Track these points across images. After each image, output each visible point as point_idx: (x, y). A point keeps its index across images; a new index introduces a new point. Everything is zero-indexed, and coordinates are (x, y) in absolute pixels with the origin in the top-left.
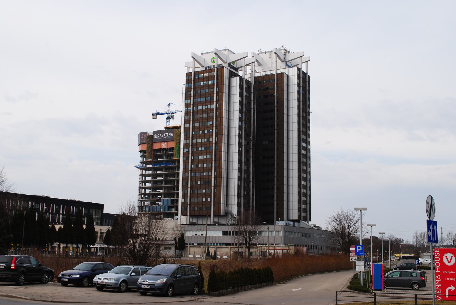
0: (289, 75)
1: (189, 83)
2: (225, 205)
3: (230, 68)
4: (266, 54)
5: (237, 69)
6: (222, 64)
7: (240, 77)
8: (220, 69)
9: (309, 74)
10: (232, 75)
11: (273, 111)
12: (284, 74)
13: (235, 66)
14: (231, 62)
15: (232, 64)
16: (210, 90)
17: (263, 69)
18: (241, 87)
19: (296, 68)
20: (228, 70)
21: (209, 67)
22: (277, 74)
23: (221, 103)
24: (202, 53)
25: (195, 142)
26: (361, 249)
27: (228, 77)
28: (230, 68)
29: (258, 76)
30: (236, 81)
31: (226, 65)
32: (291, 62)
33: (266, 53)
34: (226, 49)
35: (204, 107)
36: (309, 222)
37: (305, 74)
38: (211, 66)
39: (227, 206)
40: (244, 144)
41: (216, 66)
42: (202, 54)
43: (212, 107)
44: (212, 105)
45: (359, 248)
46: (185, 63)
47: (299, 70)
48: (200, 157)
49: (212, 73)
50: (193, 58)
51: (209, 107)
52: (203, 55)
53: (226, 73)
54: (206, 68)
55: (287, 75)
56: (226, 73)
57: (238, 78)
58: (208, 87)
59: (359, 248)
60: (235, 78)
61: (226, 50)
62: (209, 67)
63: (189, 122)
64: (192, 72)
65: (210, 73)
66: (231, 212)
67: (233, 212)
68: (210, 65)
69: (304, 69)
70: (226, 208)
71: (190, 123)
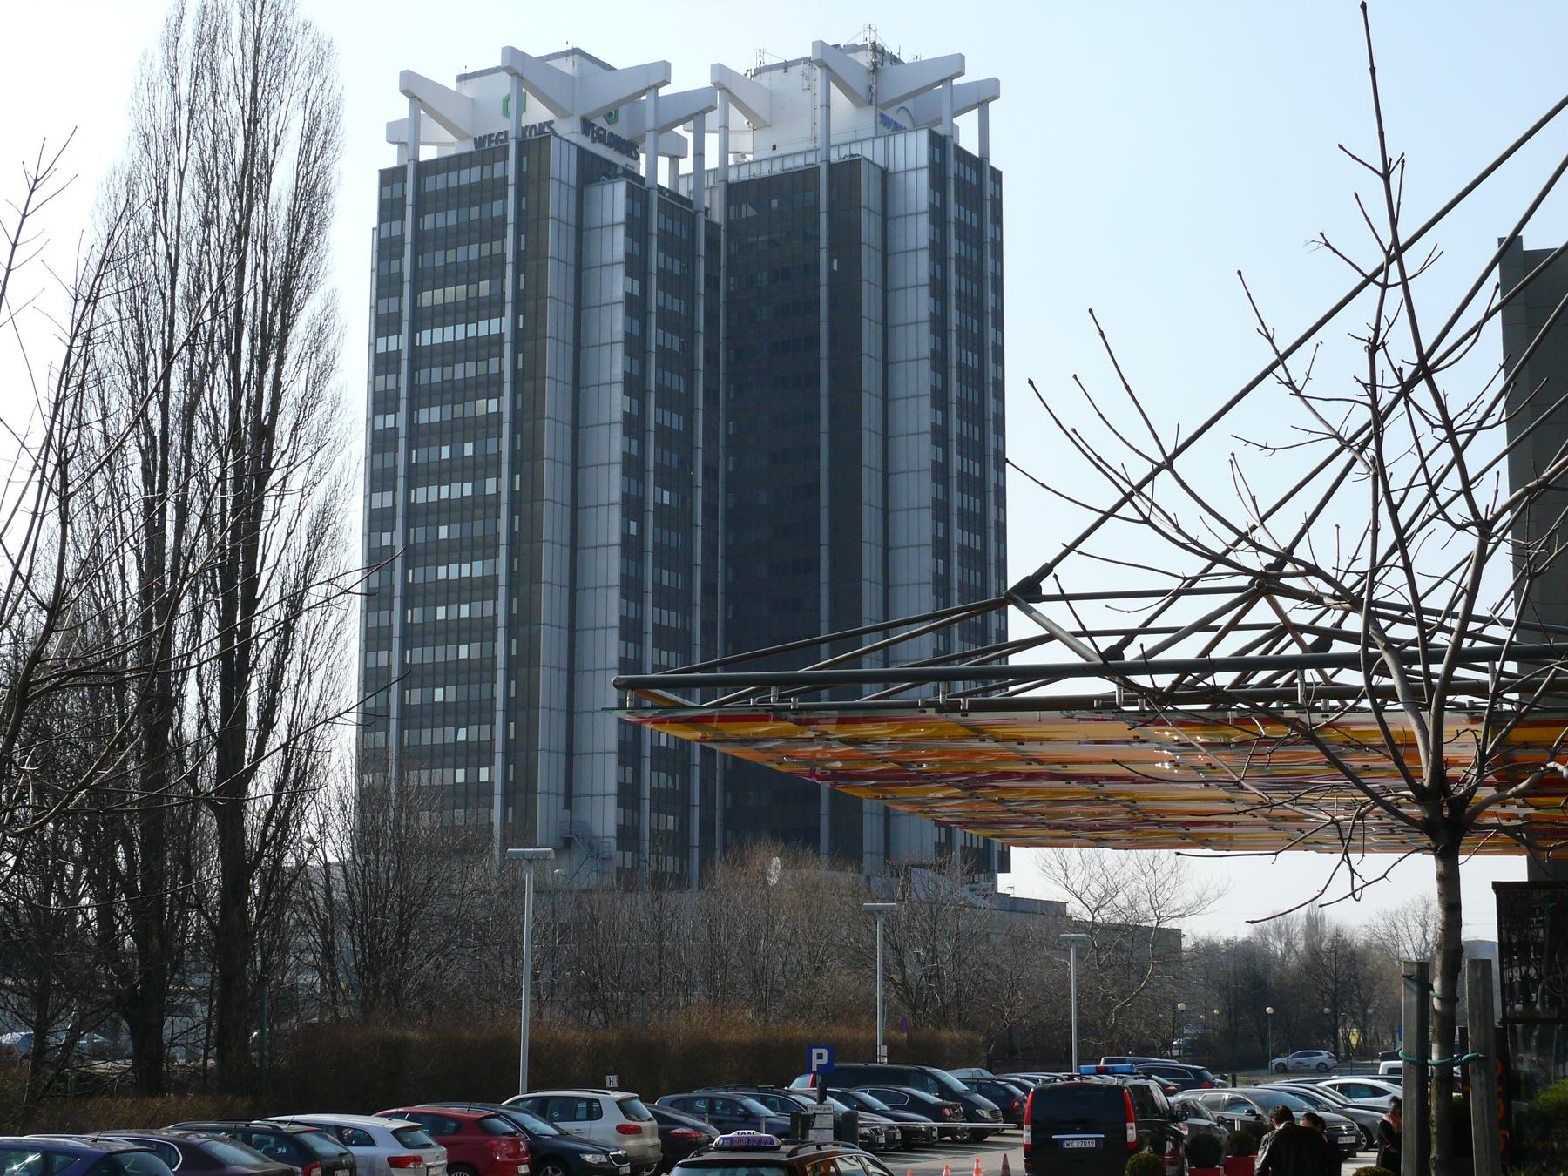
0: (891, 169)
1: (493, 200)
2: (562, 800)
3: (594, 142)
4: (786, 72)
5: (630, 148)
6: (552, 122)
7: (629, 185)
8: (535, 143)
9: (995, 161)
10: (592, 171)
11: (813, 343)
12: (863, 165)
13: (620, 130)
14: (596, 114)
15: (600, 122)
16: (486, 248)
17: (774, 148)
18: (636, 227)
19: (923, 136)
20: (574, 151)
21: (493, 138)
22: (832, 167)
23: (537, 306)
24: (463, 72)
25: (421, 499)
26: (824, 1061)
27: (573, 181)
28: (594, 142)
29: (747, 178)
30: (614, 200)
31: (568, 129)
32: (908, 104)
33: (789, 69)
34: (570, 47)
35: (460, 328)
36: (1001, 877)
37: (979, 164)
38: (500, 133)
39: (569, 805)
40: (955, 471)
41: (512, 134)
42: (462, 78)
43: (495, 330)
44: (495, 322)
45: (820, 1056)
46: (388, 124)
47: (941, 144)
48: (442, 572)
49: (498, 166)
50: (405, 92)
51: (483, 332)
52: (468, 81)
53: (562, 166)
54: (479, 142)
55: (879, 171)
56: (562, 166)
57: (620, 188)
58: (477, 235)
59: (820, 1056)
60: (608, 188)
61: (567, 54)
62: (493, 138)
63: (496, 389)
64: (406, 162)
65: (485, 168)
66: (591, 832)
67: (598, 831)
68: (496, 131)
69: (969, 142)
70: (568, 812)
71: (499, 395)
